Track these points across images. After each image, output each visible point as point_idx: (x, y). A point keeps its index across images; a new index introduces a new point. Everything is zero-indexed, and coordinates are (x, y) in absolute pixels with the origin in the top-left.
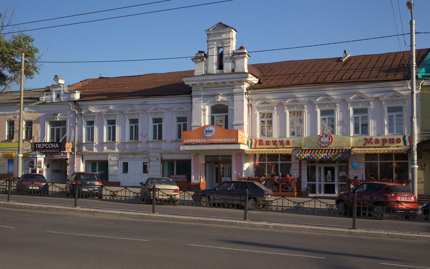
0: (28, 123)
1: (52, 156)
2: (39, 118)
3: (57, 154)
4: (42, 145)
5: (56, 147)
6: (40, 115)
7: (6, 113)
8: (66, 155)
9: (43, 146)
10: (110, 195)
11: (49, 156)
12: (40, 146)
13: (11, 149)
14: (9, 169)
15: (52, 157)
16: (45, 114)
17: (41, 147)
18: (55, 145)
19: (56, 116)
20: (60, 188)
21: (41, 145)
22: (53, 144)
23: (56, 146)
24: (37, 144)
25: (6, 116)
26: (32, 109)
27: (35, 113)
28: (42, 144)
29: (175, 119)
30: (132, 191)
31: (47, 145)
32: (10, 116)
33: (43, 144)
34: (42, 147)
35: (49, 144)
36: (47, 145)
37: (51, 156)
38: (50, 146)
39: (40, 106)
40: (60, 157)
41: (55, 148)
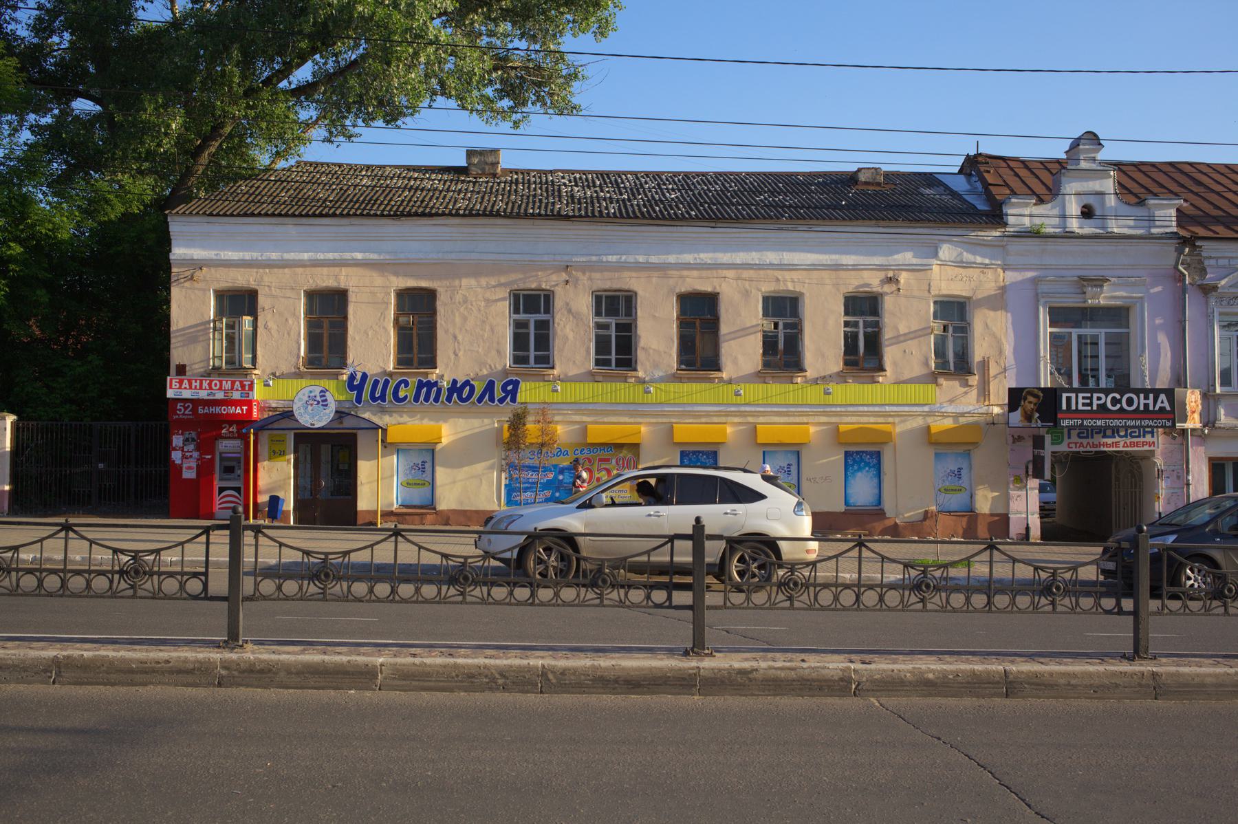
0: (770, 302)
1: (1090, 440)
2: (1003, 289)
3: (1109, 432)
4: (1091, 398)
5: (1157, 408)
6: (1012, 277)
7: (849, 260)
8: (1153, 437)
9: (1095, 402)
10: (113, 572)
11: (1074, 438)
12: (1081, 401)
13: (877, 409)
14: (849, 491)
15: (1088, 443)
16: (1030, 274)
17: (1084, 405)
18: (1151, 401)
19: (1096, 286)
20: (906, 566)
21: (1083, 398)
22: (1142, 396)
23: (1159, 404)
24: (1064, 395)
25: (842, 274)
26: (974, 254)
27: (985, 270)
28: (1089, 395)
29: (505, 307)
30: (892, 557)
31: (1113, 398)
32: (866, 274)
33: (1095, 395)
34: (1090, 404)
35: (1122, 397)
36: (1113, 398)
37: (1085, 441)
38: (1130, 401)
39: (1017, 246)
40: (1124, 447)
41: (1154, 412)
